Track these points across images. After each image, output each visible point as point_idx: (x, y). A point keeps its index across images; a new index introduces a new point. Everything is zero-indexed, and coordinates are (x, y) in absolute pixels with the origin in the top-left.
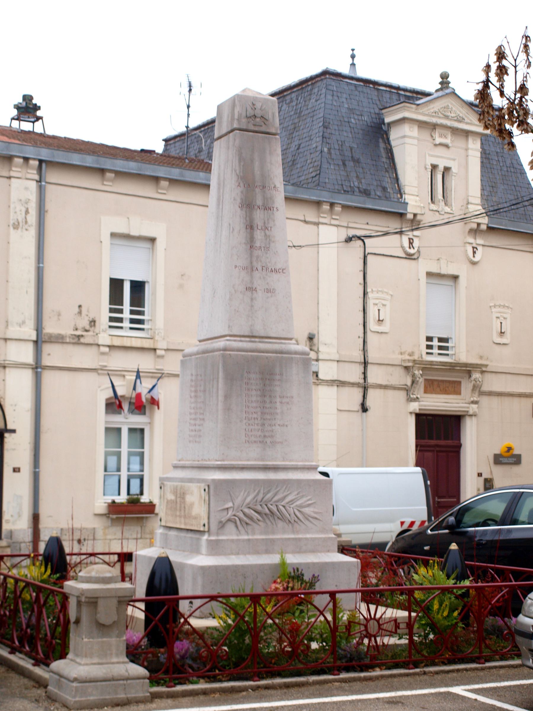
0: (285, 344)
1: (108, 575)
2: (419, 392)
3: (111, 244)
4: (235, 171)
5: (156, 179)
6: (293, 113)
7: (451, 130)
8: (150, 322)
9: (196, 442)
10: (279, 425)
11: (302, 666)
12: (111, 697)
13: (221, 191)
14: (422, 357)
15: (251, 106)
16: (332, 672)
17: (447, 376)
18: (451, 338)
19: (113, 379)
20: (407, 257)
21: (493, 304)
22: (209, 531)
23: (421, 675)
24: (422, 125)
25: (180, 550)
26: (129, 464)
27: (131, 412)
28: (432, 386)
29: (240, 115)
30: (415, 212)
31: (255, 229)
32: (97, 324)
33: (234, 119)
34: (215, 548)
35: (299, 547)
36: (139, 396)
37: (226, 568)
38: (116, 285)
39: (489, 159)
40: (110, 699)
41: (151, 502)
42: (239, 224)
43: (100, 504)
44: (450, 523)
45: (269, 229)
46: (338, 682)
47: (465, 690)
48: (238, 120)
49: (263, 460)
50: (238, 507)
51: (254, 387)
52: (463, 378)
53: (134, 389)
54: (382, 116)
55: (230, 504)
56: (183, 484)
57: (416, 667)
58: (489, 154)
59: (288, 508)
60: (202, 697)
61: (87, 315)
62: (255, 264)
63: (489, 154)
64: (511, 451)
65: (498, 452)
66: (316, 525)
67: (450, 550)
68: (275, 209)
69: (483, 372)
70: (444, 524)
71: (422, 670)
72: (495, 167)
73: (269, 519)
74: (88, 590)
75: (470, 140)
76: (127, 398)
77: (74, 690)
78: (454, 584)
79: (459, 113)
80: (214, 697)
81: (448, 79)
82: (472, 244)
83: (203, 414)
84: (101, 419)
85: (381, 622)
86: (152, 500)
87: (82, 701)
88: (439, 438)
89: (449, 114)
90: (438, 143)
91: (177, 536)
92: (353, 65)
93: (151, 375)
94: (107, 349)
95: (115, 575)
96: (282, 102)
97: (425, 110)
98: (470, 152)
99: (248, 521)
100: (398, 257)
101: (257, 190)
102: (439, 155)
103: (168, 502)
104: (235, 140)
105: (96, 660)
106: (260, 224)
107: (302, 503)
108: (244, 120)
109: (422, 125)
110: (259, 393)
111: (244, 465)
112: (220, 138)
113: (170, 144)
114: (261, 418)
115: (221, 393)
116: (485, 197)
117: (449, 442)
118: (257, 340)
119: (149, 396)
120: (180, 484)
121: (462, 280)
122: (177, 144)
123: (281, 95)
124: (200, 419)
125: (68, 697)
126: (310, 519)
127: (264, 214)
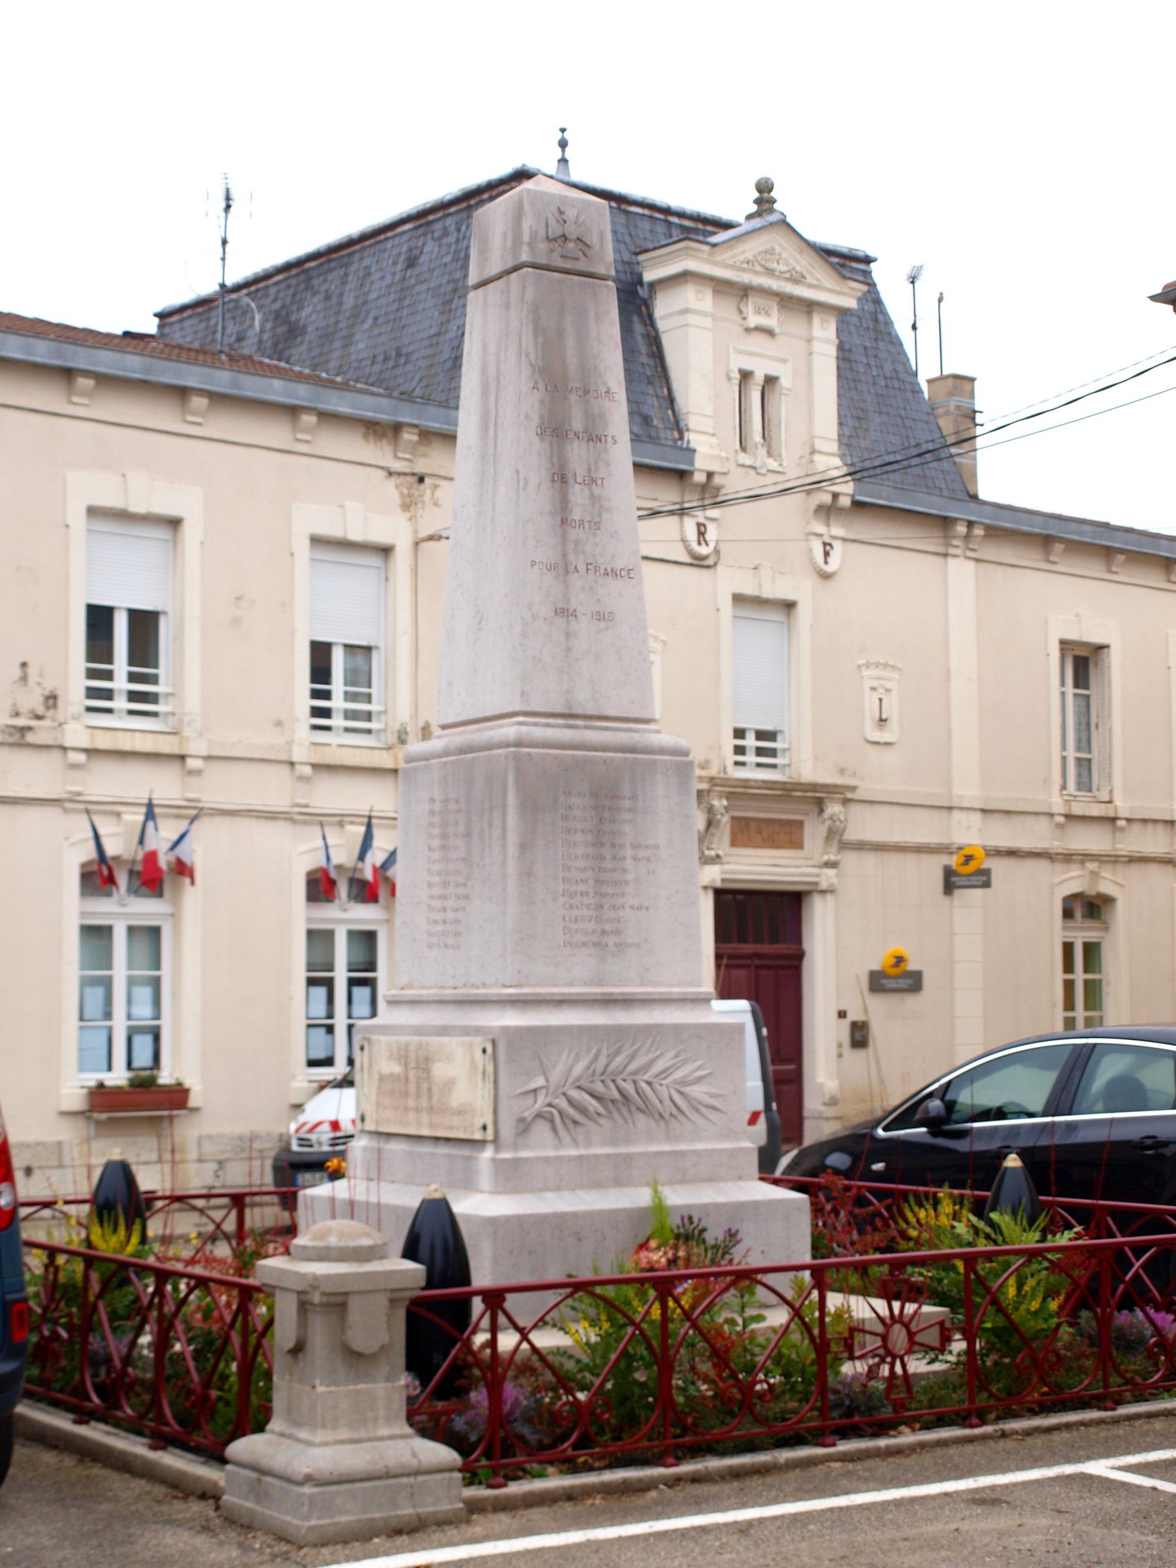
0: (637, 731)
1: (366, 1242)
2: (721, 844)
3: (89, 531)
4: (527, 355)
5: (182, 393)
6: (449, 259)
7: (777, 299)
8: (170, 698)
9: (446, 946)
10: (632, 907)
11: (757, 1429)
12: (385, 1514)
13: (492, 399)
14: (725, 773)
15: (556, 214)
16: (820, 1440)
17: (778, 810)
18: (781, 732)
19: (99, 822)
20: (695, 562)
21: (863, 662)
22: (496, 1141)
23: (998, 1437)
24: (722, 287)
25: (418, 1185)
26: (129, 1001)
27: (133, 891)
28: (748, 832)
29: (533, 235)
30: (711, 468)
31: (571, 481)
32: (60, 702)
33: (521, 243)
34: (511, 1177)
35: (684, 1169)
36: (151, 857)
37: (540, 1220)
38: (99, 619)
39: (849, 361)
40: (382, 1518)
41: (180, 1084)
42: (537, 471)
43: (73, 1088)
44: (933, 1114)
45: (599, 482)
46: (836, 1461)
47: (1120, 1468)
48: (531, 244)
49: (600, 983)
50: (557, 1089)
51: (579, 826)
52: (807, 814)
53: (141, 841)
54: (636, 267)
55: (540, 1082)
56: (424, 1039)
57: (983, 1423)
58: (850, 351)
59: (657, 1086)
60: (568, 1507)
61: (39, 684)
62: (571, 557)
63: (850, 351)
64: (902, 965)
65: (876, 967)
66: (714, 1124)
67: (1006, 1168)
68: (609, 439)
69: (846, 802)
70: (918, 1116)
71: (996, 1427)
72: (863, 379)
73: (619, 1110)
74: (327, 1277)
75: (816, 319)
76: (126, 862)
77: (306, 1503)
78: (1038, 1242)
79: (794, 264)
80: (593, 1505)
81: (772, 194)
82: (821, 535)
83: (465, 885)
84: (72, 908)
85: (913, 1328)
86: (181, 1080)
87: (322, 1526)
88: (758, 940)
89: (774, 266)
90: (752, 325)
91: (410, 1152)
92: (563, 161)
93: (174, 811)
94: (81, 758)
95: (379, 1242)
96: (425, 235)
97: (726, 256)
98: (817, 347)
99: (578, 1117)
100: (675, 562)
101: (573, 398)
102: (756, 350)
103: (382, 1078)
104: (524, 288)
105: (344, 1434)
106: (581, 472)
107: (685, 1076)
108: (542, 246)
109: (722, 287)
110: (589, 838)
111: (563, 994)
112: (478, 286)
113: (172, 324)
114: (596, 892)
115: (512, 838)
116: (845, 440)
117: (780, 948)
118: (580, 722)
119: (171, 857)
120: (416, 1038)
121: (803, 612)
122: (187, 324)
123: (422, 221)
124: (458, 897)
125: (288, 1518)
126: (703, 1110)
127: (588, 450)
